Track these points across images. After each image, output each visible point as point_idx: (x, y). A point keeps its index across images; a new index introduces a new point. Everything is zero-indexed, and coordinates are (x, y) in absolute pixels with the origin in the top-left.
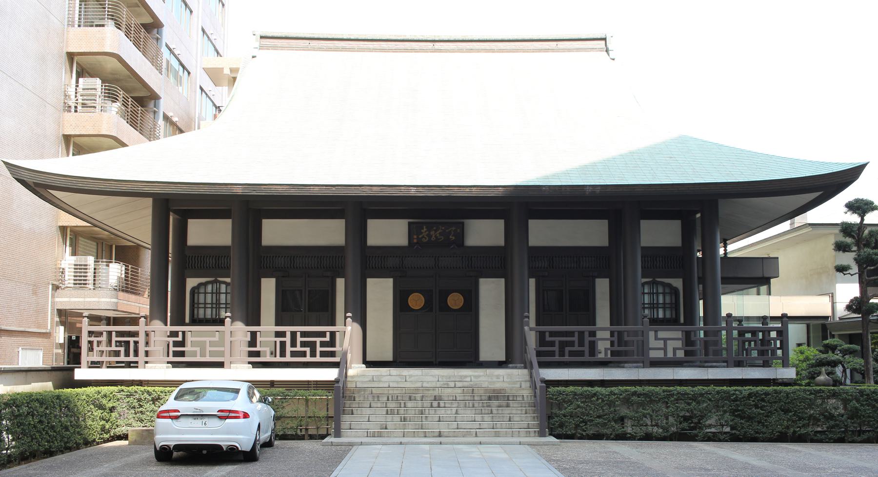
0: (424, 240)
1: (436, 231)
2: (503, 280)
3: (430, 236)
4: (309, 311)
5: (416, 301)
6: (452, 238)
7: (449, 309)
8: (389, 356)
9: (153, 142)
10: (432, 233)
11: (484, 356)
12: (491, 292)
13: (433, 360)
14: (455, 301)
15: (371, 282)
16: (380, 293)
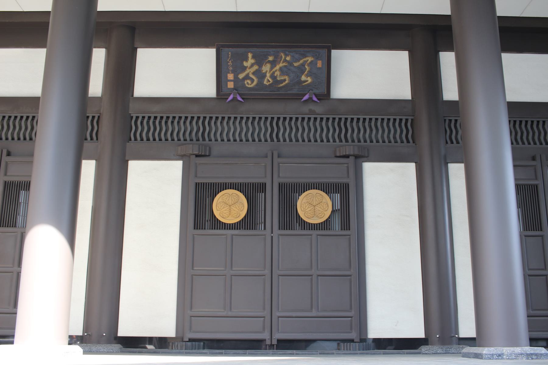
0: (249, 84)
1: (273, 64)
2: (411, 167)
3: (261, 75)
4: (196, 227)
5: (230, 206)
6: (307, 79)
7: (217, 224)
8: (167, 328)
9: (16, 339)
10: (266, 68)
11: (378, 327)
12: (388, 189)
13: (265, 336)
14: (314, 206)
15: (137, 169)
16: (156, 188)
